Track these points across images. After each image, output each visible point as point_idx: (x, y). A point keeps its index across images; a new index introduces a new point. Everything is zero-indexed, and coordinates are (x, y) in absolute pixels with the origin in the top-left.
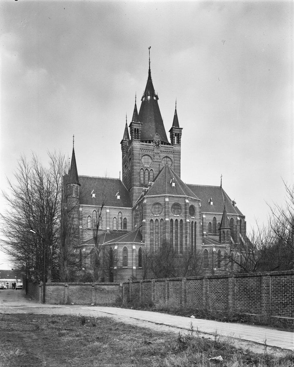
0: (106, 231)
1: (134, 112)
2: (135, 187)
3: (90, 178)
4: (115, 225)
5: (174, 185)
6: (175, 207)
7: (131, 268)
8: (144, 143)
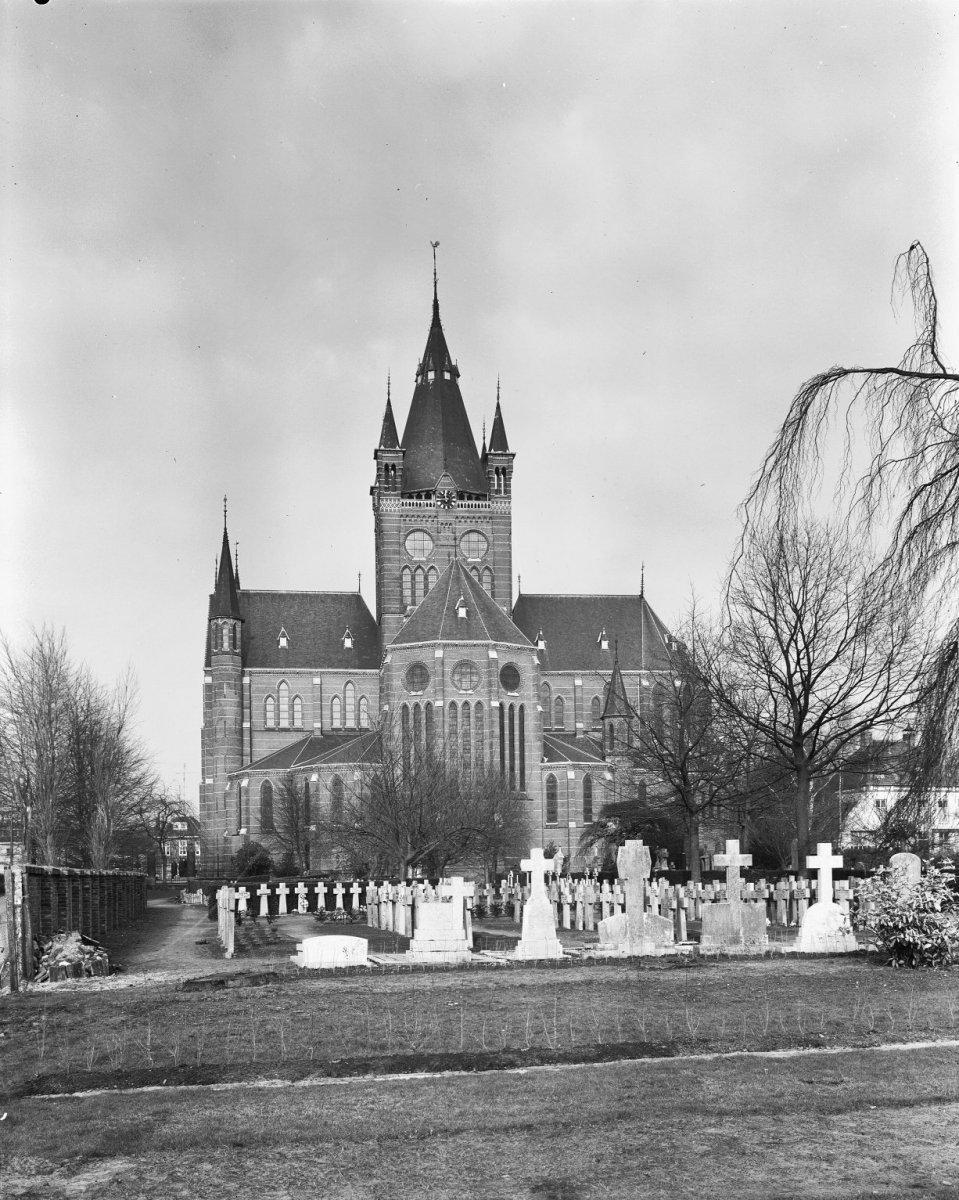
0: (312, 732)
1: (385, 420)
2: (387, 616)
3: (281, 595)
4: (337, 715)
5: (462, 613)
6: (464, 670)
7: (564, 824)
8: (415, 501)
